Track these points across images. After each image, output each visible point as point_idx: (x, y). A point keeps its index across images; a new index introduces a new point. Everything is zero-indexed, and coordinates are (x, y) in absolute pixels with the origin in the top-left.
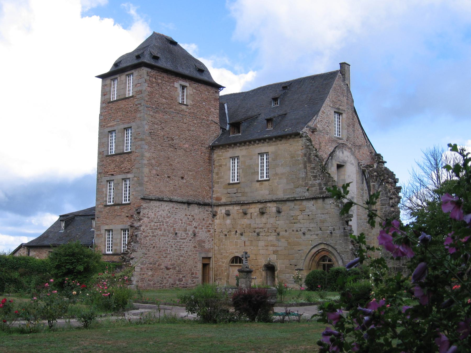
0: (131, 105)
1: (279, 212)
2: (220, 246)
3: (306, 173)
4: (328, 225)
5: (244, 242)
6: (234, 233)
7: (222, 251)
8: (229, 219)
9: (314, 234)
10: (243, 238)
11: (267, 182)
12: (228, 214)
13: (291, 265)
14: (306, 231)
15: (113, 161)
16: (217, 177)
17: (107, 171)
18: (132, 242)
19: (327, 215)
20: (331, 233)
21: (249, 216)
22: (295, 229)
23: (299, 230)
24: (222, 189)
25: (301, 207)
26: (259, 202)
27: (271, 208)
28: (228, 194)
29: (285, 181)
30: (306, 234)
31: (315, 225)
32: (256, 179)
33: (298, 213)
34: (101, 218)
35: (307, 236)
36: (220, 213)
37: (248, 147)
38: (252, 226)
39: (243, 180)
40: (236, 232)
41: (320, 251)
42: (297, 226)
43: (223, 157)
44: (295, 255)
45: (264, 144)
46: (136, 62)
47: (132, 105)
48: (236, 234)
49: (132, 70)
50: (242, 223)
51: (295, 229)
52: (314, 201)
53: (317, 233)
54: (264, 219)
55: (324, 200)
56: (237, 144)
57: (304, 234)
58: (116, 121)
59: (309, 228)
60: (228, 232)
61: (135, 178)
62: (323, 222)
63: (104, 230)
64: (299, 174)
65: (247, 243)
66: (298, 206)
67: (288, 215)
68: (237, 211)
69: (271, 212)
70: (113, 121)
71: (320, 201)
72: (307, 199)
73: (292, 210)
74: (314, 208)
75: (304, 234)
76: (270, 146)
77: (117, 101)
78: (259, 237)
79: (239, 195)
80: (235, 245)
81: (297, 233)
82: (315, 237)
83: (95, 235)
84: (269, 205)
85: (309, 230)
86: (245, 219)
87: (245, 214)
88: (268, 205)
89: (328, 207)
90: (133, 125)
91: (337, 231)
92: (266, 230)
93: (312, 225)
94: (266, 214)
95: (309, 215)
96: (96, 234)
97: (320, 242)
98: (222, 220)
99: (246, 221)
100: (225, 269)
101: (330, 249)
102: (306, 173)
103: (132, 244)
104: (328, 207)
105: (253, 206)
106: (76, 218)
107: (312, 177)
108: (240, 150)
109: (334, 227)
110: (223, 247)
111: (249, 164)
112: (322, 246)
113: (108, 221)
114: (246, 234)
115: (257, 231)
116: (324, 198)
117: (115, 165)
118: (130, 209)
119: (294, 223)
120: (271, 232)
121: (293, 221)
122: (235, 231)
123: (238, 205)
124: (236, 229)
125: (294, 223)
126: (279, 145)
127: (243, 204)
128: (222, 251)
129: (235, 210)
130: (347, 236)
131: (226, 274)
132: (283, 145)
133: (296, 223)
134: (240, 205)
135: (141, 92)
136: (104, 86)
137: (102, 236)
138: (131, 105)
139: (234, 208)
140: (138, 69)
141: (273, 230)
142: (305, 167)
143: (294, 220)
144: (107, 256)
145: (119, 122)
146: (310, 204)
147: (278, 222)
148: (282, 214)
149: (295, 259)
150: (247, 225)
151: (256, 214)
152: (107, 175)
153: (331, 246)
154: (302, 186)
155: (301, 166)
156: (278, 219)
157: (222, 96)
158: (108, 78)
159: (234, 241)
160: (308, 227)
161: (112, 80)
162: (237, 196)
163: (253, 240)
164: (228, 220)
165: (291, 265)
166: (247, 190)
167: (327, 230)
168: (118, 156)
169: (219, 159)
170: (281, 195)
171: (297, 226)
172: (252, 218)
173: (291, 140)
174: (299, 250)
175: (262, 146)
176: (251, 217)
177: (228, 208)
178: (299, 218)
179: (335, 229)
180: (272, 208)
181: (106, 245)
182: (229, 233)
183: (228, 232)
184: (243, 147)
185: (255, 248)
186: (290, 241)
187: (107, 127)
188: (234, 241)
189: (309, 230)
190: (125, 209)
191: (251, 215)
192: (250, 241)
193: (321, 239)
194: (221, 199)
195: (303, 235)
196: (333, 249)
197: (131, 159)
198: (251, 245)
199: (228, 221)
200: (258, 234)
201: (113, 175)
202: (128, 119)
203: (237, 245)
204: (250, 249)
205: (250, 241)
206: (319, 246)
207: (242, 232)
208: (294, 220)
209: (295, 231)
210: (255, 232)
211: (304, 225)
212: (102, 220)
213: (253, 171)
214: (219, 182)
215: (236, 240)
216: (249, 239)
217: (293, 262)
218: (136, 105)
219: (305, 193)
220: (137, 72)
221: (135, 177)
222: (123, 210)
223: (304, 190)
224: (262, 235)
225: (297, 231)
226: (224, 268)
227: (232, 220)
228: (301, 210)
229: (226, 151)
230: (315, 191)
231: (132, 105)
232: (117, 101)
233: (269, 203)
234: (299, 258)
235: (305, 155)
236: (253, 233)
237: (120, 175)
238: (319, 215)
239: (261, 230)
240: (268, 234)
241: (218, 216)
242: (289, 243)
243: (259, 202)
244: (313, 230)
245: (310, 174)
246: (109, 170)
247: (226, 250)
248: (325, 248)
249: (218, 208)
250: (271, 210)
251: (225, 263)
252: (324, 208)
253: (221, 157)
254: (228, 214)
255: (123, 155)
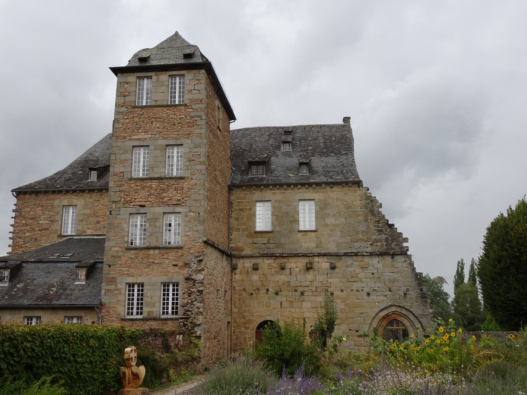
0: (181, 116)
1: (333, 268)
2: (242, 307)
3: (368, 227)
4: (401, 285)
5: (279, 303)
6: (265, 291)
7: (244, 314)
8: (256, 274)
9: (382, 295)
10: (278, 298)
11: (313, 234)
12: (255, 268)
13: (350, 330)
14: (370, 292)
15: (143, 188)
16: (236, 222)
17: (131, 200)
18: (195, 301)
19: (398, 274)
20: (405, 294)
21: (287, 271)
22: (355, 289)
23: (360, 290)
24: (245, 238)
25: (361, 263)
26: (305, 256)
27: (320, 264)
28: (255, 245)
29: (339, 233)
30: (371, 295)
31: (383, 285)
32: (297, 230)
33: (358, 270)
34: (117, 266)
35: (373, 297)
36: (241, 266)
37: (290, 191)
38: (292, 284)
39: (277, 229)
40: (268, 290)
41: (389, 314)
42: (356, 286)
43: (246, 199)
44: (356, 319)
45: (307, 190)
46: (182, 61)
47: (183, 116)
48: (267, 293)
49: (185, 70)
50: (277, 280)
51: (355, 289)
52: (380, 257)
53: (385, 293)
54: (310, 276)
55: (392, 258)
56: (305, 185)
57: (369, 294)
58: (150, 133)
59: (376, 288)
60: (255, 290)
61: (191, 213)
62: (393, 281)
63: (125, 284)
64: (358, 227)
65: (284, 304)
66: (358, 263)
67: (344, 272)
68: (269, 266)
69: (320, 267)
70: (143, 134)
71: (388, 259)
72: (371, 254)
73: (350, 267)
74: (380, 265)
75: (369, 294)
76: (316, 192)
77: (152, 107)
78: (303, 297)
79: (272, 246)
80: (266, 306)
81: (358, 293)
82: (382, 298)
83: (103, 291)
84: (316, 259)
85: (374, 290)
86: (282, 276)
87: (283, 268)
88: (315, 259)
89: (399, 265)
90: (187, 142)
91: (411, 292)
92: (314, 289)
93: (378, 285)
94: (314, 271)
95: (373, 274)
96: (105, 290)
97: (390, 303)
98: (245, 276)
99: (282, 278)
100: (250, 336)
101: (404, 312)
102: (368, 227)
103: (195, 304)
104: (399, 265)
105: (294, 260)
106: (24, 265)
107: (376, 231)
108: (273, 193)
109: (407, 287)
110: (247, 309)
111: (287, 211)
112: (394, 309)
113: (132, 270)
114: (283, 293)
115: (300, 289)
116: (393, 255)
117: (148, 193)
118: (181, 256)
119: (354, 282)
120: (321, 291)
121: (353, 279)
122: (266, 289)
123: (270, 258)
124: (268, 287)
125: (354, 282)
126: (329, 193)
127: (281, 256)
128: (244, 314)
129: (265, 263)
130: (426, 297)
131: (252, 342)
132: (334, 193)
133: (356, 282)
134: (274, 258)
135: (201, 101)
136: (120, 85)
137: (120, 294)
138: (181, 116)
139: (264, 261)
140: (194, 71)
141: (324, 289)
142: (366, 220)
143: (354, 278)
144: (130, 322)
145: (157, 136)
146: (375, 260)
147: (330, 280)
148: (337, 270)
149: (357, 324)
150: (284, 282)
151: (297, 269)
152: (132, 206)
153: (405, 308)
154: (363, 240)
155: (360, 218)
156: (330, 277)
157: (234, 131)
158: (132, 74)
159: (265, 302)
160: (374, 286)
161: (170, 76)
162: (268, 247)
163: (293, 299)
164: (255, 276)
165: (350, 330)
166: (283, 241)
167: (399, 291)
168: (154, 181)
169: (238, 202)
170: (332, 248)
171: (356, 286)
172: (292, 274)
173: (346, 189)
174: (361, 313)
175: (305, 192)
176: (290, 273)
177: (254, 261)
178: (360, 276)
179: (409, 290)
180: (323, 264)
181: (125, 306)
182: (256, 292)
183: (255, 290)
184: (277, 191)
185: (296, 310)
186: (347, 302)
187: (130, 140)
188: (265, 302)
189: (374, 290)
190: (172, 255)
191: (290, 271)
192: (290, 301)
193: (391, 301)
194: (243, 250)
195: (366, 295)
196: (408, 312)
197: (182, 189)
198: (291, 306)
199: (255, 277)
200: (302, 294)
201: (144, 206)
202: (176, 133)
203: (270, 307)
204: (289, 311)
205: (290, 301)
206: (389, 308)
207: (278, 290)
208: (354, 278)
209: (355, 291)
210: (296, 291)
211: (368, 285)
212: (119, 269)
213: (293, 219)
214: (240, 229)
215: (267, 301)
216: (288, 299)
217: (355, 326)
218: (192, 117)
219: (367, 248)
220: (193, 74)
221: (190, 211)
222: (166, 257)
223: (366, 245)
224: (308, 294)
225: (357, 291)
226: (249, 335)
227: (261, 276)
228: (362, 267)
229: (250, 193)
230: (379, 247)
231: (183, 116)
232: (146, 107)
233: (317, 257)
234: (362, 323)
235: (366, 206)
236: (294, 293)
237: (158, 207)
238: (388, 273)
239: (306, 289)
240: (316, 293)
241: (238, 271)
242: (346, 305)
243: (305, 256)
244: (379, 290)
245: (373, 228)
246: (135, 199)
247: (252, 313)
248: (398, 311)
249: (238, 260)
250: (320, 265)
251: (250, 329)
252: (393, 266)
253: (242, 199)
254: (255, 268)
255: (166, 180)
